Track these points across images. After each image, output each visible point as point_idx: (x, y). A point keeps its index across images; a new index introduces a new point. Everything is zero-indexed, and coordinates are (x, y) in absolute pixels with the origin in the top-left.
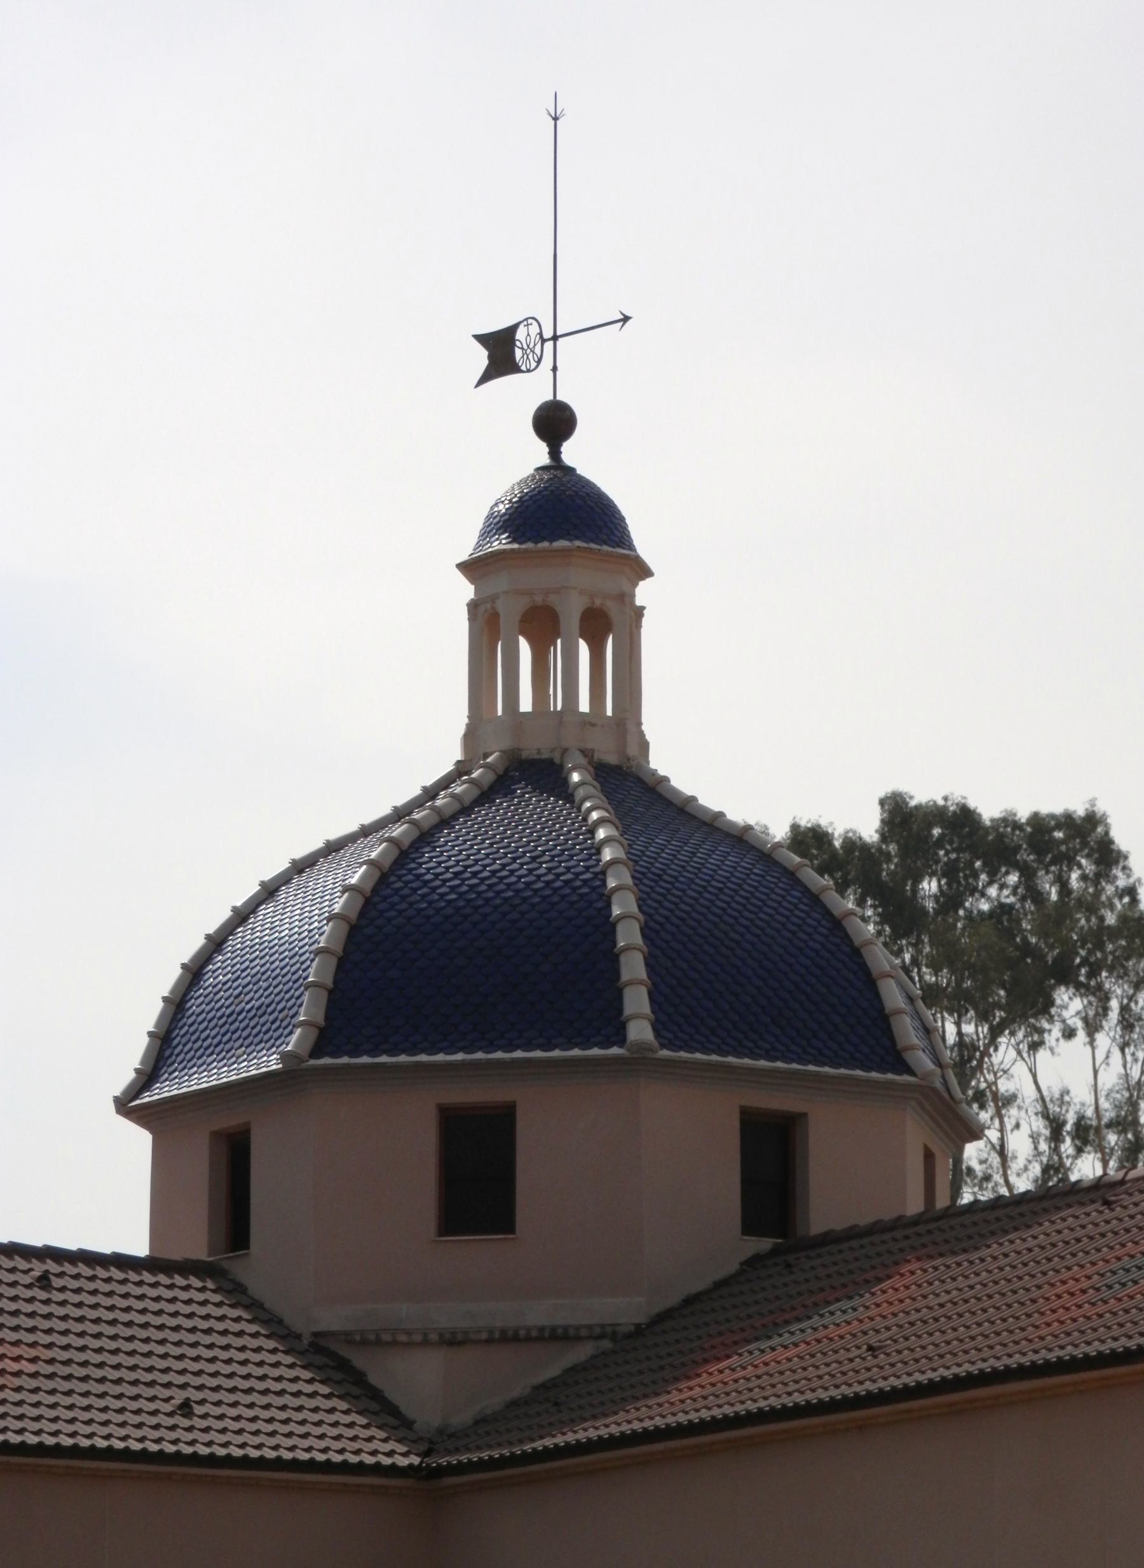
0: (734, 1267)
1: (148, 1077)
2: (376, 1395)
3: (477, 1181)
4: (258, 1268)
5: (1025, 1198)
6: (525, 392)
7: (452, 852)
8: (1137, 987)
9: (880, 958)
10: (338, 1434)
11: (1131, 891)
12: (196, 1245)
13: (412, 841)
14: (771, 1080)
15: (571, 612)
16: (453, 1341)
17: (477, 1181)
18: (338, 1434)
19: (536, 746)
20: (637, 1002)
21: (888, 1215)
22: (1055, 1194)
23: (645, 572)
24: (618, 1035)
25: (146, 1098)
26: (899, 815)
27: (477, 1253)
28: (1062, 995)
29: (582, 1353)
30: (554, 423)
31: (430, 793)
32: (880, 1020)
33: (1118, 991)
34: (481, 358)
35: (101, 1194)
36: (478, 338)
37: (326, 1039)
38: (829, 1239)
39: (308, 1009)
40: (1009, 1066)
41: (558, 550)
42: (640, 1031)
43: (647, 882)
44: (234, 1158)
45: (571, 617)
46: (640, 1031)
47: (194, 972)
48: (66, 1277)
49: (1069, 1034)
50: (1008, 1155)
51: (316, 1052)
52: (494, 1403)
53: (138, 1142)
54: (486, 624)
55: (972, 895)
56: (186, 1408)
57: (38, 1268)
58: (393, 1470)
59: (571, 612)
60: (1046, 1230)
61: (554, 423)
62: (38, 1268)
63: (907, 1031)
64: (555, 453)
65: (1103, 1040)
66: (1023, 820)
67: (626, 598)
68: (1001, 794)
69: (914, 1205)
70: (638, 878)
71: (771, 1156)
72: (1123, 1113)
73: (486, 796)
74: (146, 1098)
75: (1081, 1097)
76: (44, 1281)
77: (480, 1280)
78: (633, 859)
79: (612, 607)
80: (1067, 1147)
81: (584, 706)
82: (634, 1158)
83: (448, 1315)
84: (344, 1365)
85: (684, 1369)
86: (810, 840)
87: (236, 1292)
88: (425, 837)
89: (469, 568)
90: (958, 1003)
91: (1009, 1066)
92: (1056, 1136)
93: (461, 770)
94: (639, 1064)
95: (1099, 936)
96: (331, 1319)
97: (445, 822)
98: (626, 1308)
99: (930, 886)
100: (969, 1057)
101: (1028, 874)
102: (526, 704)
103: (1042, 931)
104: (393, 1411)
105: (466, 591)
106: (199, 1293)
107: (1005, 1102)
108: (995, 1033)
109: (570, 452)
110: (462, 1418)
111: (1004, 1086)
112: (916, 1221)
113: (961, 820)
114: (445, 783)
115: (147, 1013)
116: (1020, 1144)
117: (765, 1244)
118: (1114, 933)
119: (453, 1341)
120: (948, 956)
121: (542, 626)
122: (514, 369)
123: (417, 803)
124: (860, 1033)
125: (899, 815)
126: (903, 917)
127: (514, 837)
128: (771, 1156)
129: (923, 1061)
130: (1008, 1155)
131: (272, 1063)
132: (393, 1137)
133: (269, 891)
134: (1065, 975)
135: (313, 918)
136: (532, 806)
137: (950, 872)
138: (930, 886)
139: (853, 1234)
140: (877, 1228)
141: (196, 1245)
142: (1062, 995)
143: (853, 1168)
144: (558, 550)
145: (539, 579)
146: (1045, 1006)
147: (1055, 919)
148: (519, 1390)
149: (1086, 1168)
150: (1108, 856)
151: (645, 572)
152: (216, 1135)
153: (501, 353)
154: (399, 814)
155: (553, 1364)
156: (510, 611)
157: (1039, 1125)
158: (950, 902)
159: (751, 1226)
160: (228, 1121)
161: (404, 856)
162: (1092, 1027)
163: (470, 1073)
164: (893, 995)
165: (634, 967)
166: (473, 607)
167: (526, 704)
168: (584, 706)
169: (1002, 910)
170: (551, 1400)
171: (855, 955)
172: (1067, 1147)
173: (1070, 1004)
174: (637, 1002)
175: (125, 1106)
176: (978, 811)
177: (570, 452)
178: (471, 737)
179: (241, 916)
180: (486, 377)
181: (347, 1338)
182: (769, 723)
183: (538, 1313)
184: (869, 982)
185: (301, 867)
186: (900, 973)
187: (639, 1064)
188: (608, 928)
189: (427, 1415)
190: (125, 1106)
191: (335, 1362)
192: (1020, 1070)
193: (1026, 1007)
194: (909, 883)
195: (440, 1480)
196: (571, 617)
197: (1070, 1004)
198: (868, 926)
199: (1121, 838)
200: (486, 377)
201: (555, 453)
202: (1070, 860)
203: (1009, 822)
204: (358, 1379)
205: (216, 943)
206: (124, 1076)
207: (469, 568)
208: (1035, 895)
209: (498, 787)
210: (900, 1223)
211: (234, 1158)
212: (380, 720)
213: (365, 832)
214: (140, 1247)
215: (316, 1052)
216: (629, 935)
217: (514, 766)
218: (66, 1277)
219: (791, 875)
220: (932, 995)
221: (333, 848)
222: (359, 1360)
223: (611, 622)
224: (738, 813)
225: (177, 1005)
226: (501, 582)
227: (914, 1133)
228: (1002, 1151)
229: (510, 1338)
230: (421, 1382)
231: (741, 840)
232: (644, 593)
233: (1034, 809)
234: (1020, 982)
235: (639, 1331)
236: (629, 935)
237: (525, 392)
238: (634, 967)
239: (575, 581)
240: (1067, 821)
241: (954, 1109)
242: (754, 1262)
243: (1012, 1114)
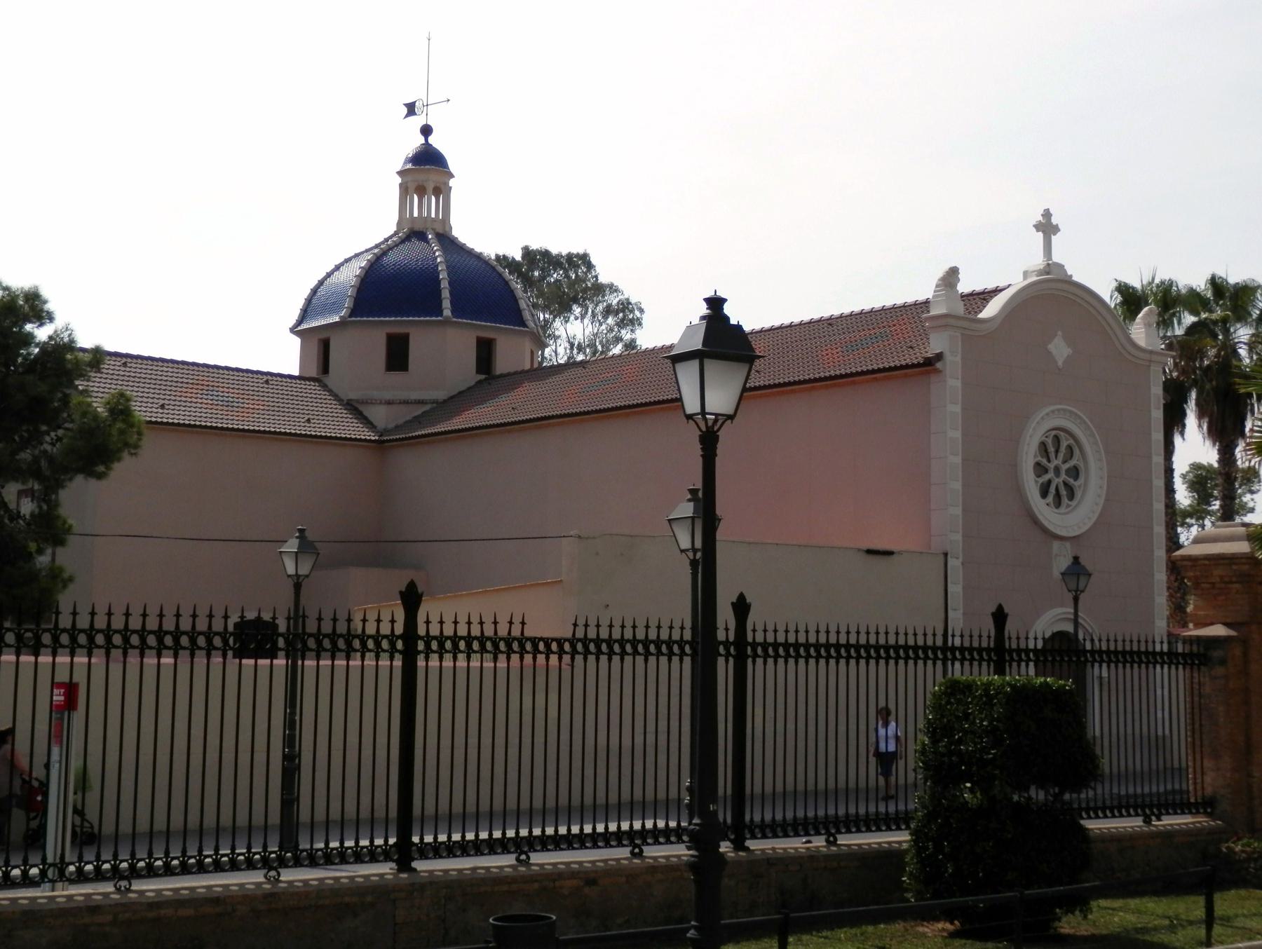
0: (473, 383)
1: (300, 322)
2: (366, 418)
3: (397, 355)
4: (331, 380)
5: (560, 365)
6: (418, 121)
7: (392, 258)
11: (596, 277)
12: (313, 373)
13: (380, 255)
14: (487, 329)
15: (430, 187)
16: (389, 403)
17: (397, 355)
19: (418, 227)
20: (446, 304)
21: (520, 369)
22: (571, 364)
23: (452, 176)
24: (439, 312)
25: (304, 326)
26: (527, 252)
27: (397, 377)
28: (575, 307)
29: (427, 407)
30: (426, 131)
31: (386, 240)
32: (519, 312)
33: (591, 307)
34: (405, 110)
35: (285, 357)
37: (354, 312)
38: (502, 376)
39: (348, 303)
40: (558, 326)
41: (427, 167)
42: (447, 312)
43: (451, 269)
44: (325, 346)
45: (430, 189)
46: (447, 312)
47: (314, 291)
48: (274, 381)
49: (576, 318)
50: (557, 353)
51: (350, 316)
52: (401, 422)
53: (296, 341)
54: (405, 190)
55: (1197, 520)
56: (309, 421)
57: (265, 378)
58: (370, 441)
59: (430, 187)
60: (566, 374)
61: (426, 131)
62: (265, 378)
63: (527, 315)
64: (426, 140)
65: (586, 321)
66: (1203, 287)
67: (447, 184)
68: (559, 247)
69: (527, 367)
70: (448, 267)
71: (485, 350)
72: (540, 301)
73: (403, 241)
74: (304, 326)
75: (580, 337)
76: (267, 382)
77: (397, 385)
78: (446, 261)
79: (442, 187)
80: (575, 351)
81: (433, 215)
82: (445, 350)
83: (388, 395)
84: (356, 409)
85: (458, 412)
86: (503, 260)
87: (325, 387)
88: (384, 253)
89: (400, 173)
90: (545, 308)
91: (558, 326)
92: (572, 345)
93: (396, 233)
94: (446, 322)
95: (586, 290)
96: (353, 395)
97: (391, 249)
98: (441, 395)
99: (536, 274)
100: (547, 325)
101: (566, 271)
102: (416, 214)
103: (569, 288)
104: (371, 423)
105: (399, 180)
106: (313, 386)
107: (556, 338)
108: (555, 317)
109: (431, 140)
110: (391, 426)
111: (557, 333)
112: (528, 371)
113: (546, 254)
114: (391, 237)
115: (300, 303)
116: (561, 350)
117: (483, 377)
118: (590, 289)
119: (389, 403)
120: (541, 294)
121: (421, 191)
122: (414, 114)
123: (382, 243)
124: (510, 313)
125: (527, 252)
126: (528, 282)
127: (411, 254)
128: (485, 350)
129: (531, 324)
131: (337, 319)
132: (370, 343)
133: (337, 268)
134: (575, 300)
135: (351, 274)
136: (417, 245)
137: (543, 270)
138: (536, 274)
139: (509, 375)
140: (516, 373)
141: (313, 373)
142: (575, 307)
144: (427, 167)
145: (421, 177)
146: (570, 310)
147: (572, 284)
148: (408, 418)
149: (580, 357)
150: (590, 266)
151: (452, 176)
152: (320, 340)
153: (411, 109)
154: (377, 246)
155: (419, 410)
156: (412, 186)
157: (567, 345)
158: (542, 278)
159: (479, 371)
160: (324, 335)
161: (378, 258)
162: (583, 317)
163: (395, 323)
164: (523, 304)
165: (446, 294)
166: (401, 185)
167: (416, 214)
168: (433, 215)
169: (557, 281)
170: (418, 421)
172: (575, 351)
173: (577, 310)
174: (446, 304)
175: (292, 330)
177: (431, 140)
178: (399, 224)
179: (329, 275)
180: (407, 116)
181: (357, 401)
182: (488, 224)
183: (414, 396)
184: (515, 300)
185: (347, 261)
187: (446, 322)
188: (438, 282)
190: (292, 330)
191: (354, 408)
192: (562, 329)
195: (383, 445)
196: (430, 189)
197: (577, 310)
198: (518, 286)
199: (594, 261)
200: (407, 116)
201: (426, 140)
202: (578, 266)
203: (560, 255)
204: (361, 413)
205: (321, 283)
206: (293, 321)
207: (400, 173)
208: (568, 277)
209: (407, 238)
210: (523, 372)
211: (325, 346)
212: (368, 219)
213: (367, 251)
214: (296, 372)
215: (350, 316)
217: (412, 233)
218: (274, 381)
219: (493, 268)
220: (535, 306)
221: (357, 255)
222: (361, 408)
223: (442, 191)
224: (478, 248)
225: (309, 301)
226: (409, 178)
227: (528, 345)
228: (556, 352)
229: (406, 402)
230: (379, 415)
231: (479, 257)
232: (452, 182)
234: (562, 303)
235: (445, 401)
236: (445, 284)
237: (418, 121)
238: (446, 294)
239: (430, 177)
240: (578, 255)
241: (540, 338)
242: (480, 382)
243: (559, 341)
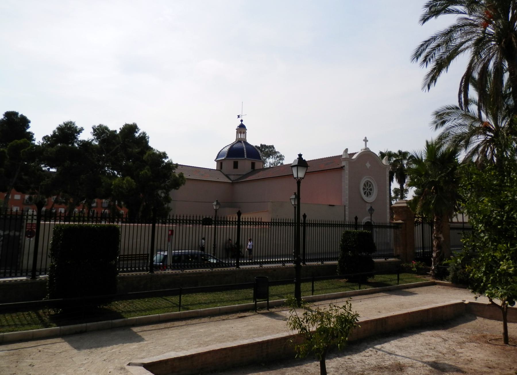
3: (236, 165)
4: (222, 170)
6: (240, 119)
7: (235, 146)
8: (477, 3)
9: (260, 153)
10: (227, 180)
12: (219, 169)
14: (253, 160)
17: (236, 165)
18: (227, 180)
20: (245, 155)
22: (270, 167)
26: (261, 145)
27: (236, 170)
30: (242, 121)
32: (260, 157)
35: (213, 166)
36: (300, 155)
37: (227, 157)
40: (267, 160)
41: (242, 128)
44: (221, 164)
50: (267, 165)
53: (216, 163)
54: (237, 133)
61: (242, 121)
68: (268, 144)
71: (253, 165)
82: (245, 165)
83: (234, 173)
86: (256, 146)
87: (221, 172)
91: (267, 160)
94: (245, 159)
96: (227, 173)
98: (244, 173)
120: (264, 153)
121: (241, 133)
124: (258, 157)
125: (261, 145)
126: (261, 151)
127: (239, 145)
128: (253, 165)
130: (267, 165)
132: (231, 163)
135: (226, 149)
141: (219, 169)
143: (258, 166)
144: (242, 128)
145: (240, 130)
147: (270, 152)
150: (274, 148)
153: (239, 116)
165: (245, 153)
170: (240, 179)
171: (258, 153)
174: (245, 155)
176: (122, 127)
180: (300, 155)
182: (254, 139)
183: (239, 174)
186: (261, 154)
187: (245, 159)
189: (232, 179)
191: (227, 176)
193: (268, 156)
194: (492, 135)
195: (233, 183)
197: (271, 157)
198: (259, 151)
211: (221, 164)
212: (230, 138)
216: (245, 151)
217: (239, 141)
223: (245, 133)
225: (218, 155)
227: (261, 164)
230: (232, 177)
231: (252, 146)
233: (73, 121)
234: (268, 155)
236: (245, 151)
237: (240, 119)
238: (245, 153)
239: (243, 130)
241: (264, 162)
